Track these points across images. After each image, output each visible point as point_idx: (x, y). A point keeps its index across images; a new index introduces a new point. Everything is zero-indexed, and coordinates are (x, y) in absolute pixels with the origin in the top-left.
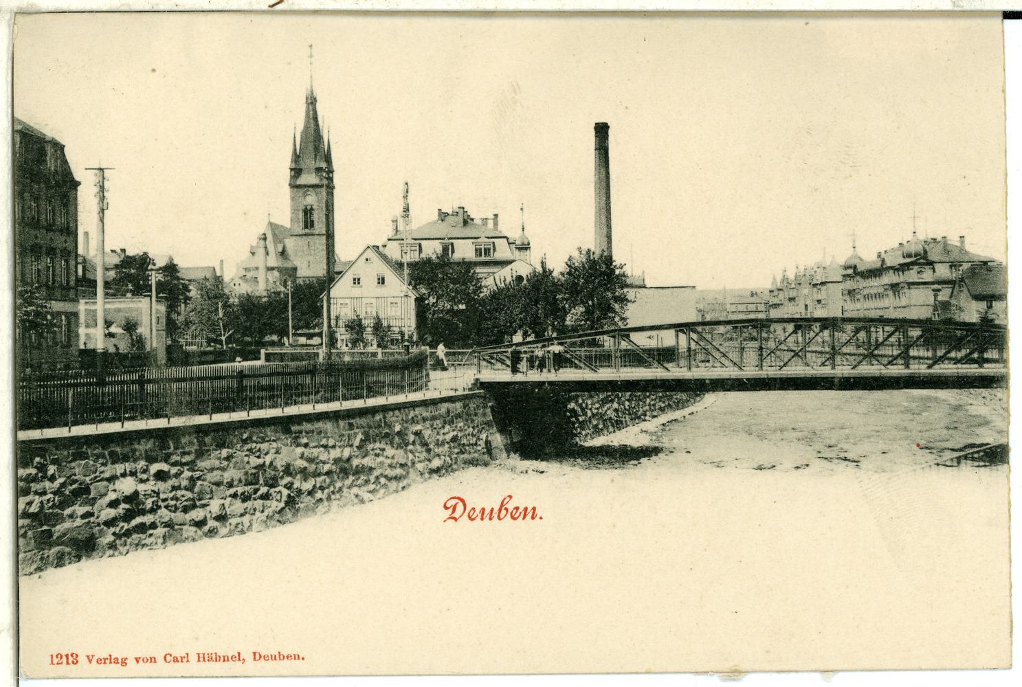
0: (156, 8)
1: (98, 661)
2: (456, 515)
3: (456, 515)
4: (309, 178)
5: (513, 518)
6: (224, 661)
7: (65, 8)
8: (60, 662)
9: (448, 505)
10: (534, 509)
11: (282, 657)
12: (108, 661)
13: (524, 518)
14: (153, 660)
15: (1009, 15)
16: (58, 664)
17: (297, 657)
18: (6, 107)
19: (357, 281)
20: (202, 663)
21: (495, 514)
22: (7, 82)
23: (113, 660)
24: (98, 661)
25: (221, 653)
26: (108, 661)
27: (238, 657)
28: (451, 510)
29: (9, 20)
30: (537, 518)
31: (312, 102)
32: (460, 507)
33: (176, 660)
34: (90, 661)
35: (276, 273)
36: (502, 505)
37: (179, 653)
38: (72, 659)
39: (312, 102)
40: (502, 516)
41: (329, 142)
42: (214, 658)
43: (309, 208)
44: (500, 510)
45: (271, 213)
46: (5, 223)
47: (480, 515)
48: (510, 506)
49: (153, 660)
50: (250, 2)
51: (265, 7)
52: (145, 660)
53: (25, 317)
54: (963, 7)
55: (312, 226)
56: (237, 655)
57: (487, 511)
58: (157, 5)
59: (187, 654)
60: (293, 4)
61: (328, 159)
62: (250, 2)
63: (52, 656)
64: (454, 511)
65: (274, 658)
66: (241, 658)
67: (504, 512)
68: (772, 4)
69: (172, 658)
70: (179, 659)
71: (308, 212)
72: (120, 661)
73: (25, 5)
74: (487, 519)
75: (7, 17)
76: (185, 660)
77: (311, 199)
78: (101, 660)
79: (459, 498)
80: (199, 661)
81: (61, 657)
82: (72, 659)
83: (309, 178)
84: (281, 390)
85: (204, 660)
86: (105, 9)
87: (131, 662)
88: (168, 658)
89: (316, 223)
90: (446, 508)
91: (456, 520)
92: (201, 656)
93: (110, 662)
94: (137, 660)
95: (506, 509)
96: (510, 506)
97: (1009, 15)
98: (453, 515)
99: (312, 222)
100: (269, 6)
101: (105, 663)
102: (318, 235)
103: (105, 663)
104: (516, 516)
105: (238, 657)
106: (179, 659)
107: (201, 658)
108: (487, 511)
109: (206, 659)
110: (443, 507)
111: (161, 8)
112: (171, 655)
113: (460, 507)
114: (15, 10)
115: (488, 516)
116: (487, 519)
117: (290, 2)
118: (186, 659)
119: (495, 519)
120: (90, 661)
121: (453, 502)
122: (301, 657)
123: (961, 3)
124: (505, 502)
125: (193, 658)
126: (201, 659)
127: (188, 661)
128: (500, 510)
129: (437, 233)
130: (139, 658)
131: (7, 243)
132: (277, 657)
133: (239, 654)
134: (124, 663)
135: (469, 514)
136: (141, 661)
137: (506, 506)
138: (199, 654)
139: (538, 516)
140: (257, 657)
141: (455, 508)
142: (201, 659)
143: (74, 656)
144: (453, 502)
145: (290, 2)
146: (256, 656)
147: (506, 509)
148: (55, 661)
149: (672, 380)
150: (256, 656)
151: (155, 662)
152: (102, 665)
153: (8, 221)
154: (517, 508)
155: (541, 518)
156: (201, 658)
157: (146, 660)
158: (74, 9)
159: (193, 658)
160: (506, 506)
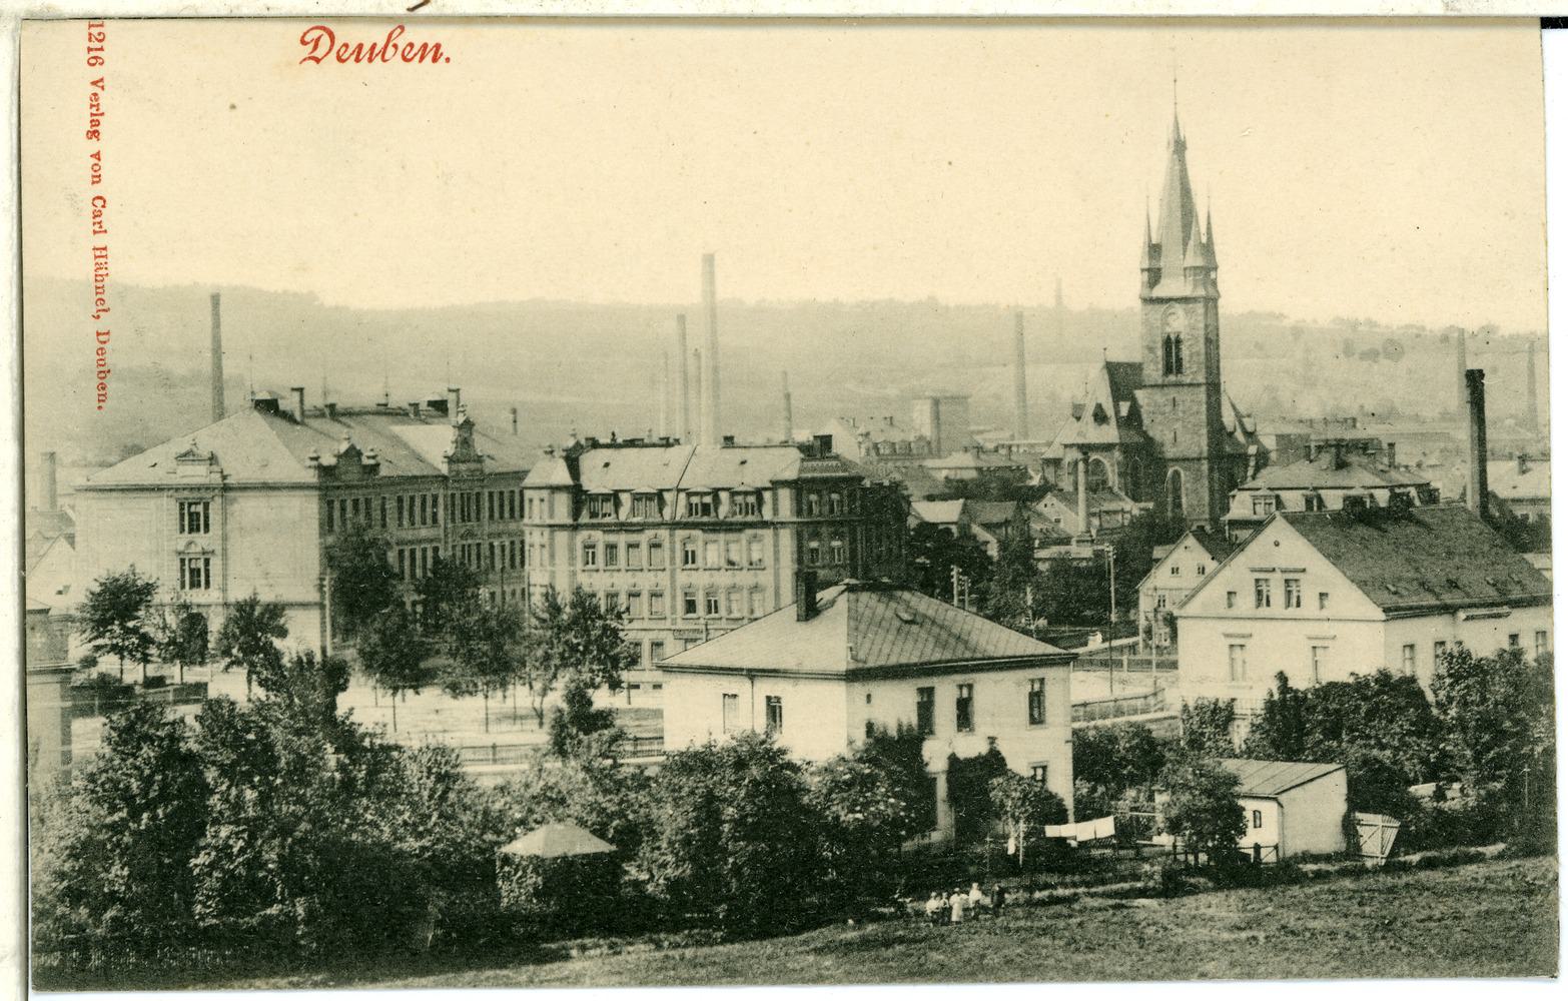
2: (319, 53)
3: (319, 53)
6: (97, 288)
9: (308, 38)
12: (94, 110)
14: (96, 179)
16: (90, 34)
19: (1175, 571)
20: (91, 254)
23: (95, 118)
30: (442, 59)
33: (97, 215)
41: (1209, 223)
42: (100, 272)
43: (1173, 337)
48: (402, 42)
49: (96, 179)
50: (379, 4)
52: (96, 168)
55: (1179, 370)
57: (366, 49)
58: (238, 7)
62: (379, 4)
64: (316, 48)
66: (100, 313)
67: (390, 50)
69: (99, 208)
70: (98, 220)
74: (365, 61)
77: (1179, 322)
78: (103, 389)
85: (96, 257)
87: (94, 146)
88: (99, 203)
89: (1186, 364)
90: (304, 42)
91: (318, 60)
92: (104, 253)
93: (92, 115)
95: (395, 46)
96: (402, 42)
99: (1179, 360)
101: (92, 106)
102: (1190, 385)
103: (92, 106)
104: (409, 57)
106: (98, 220)
108: (366, 49)
109: (98, 260)
112: (104, 206)
113: (326, 39)
115: (432, 53)
116: (365, 61)
117: (440, 3)
118: (98, 230)
120: (94, 83)
121: (316, 34)
122: (101, 404)
124: (394, 36)
125: (101, 241)
126: (98, 253)
127: (95, 232)
130: (99, 159)
132: (102, 369)
138: (105, 249)
140: (102, 338)
142: (98, 253)
143: (101, 37)
144: (316, 34)
145: (440, 3)
147: (395, 46)
151: (93, 183)
157: (96, 168)
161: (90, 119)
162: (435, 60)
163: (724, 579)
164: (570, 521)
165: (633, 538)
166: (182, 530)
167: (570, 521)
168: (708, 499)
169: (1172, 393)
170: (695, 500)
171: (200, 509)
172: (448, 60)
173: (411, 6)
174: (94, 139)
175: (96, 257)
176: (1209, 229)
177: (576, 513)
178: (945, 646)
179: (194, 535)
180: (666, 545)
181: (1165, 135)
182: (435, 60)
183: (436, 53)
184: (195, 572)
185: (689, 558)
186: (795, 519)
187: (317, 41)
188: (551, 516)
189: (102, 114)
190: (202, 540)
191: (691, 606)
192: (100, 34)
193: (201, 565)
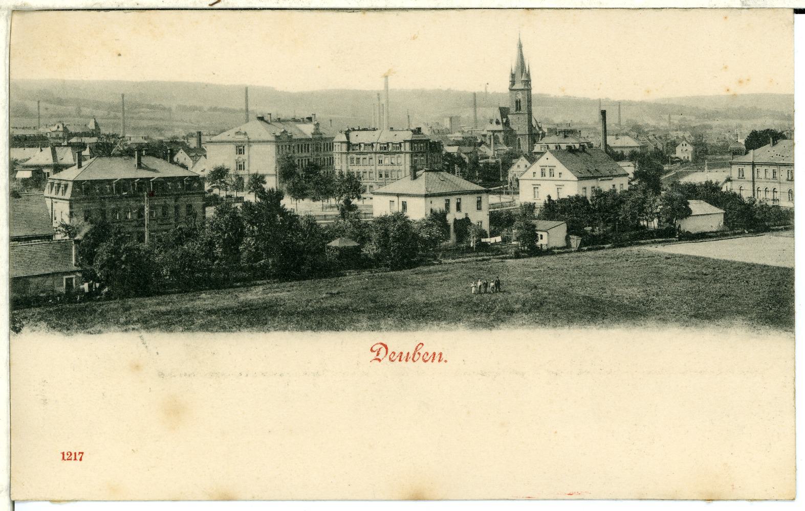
0: (121, 7)
3: (379, 357)
4: (518, 86)
8: (70, 458)
9: (374, 349)
10: (441, 354)
13: (432, 361)
15: (797, 11)
16: (68, 459)
19: (518, 166)
28: (376, 353)
29: (7, 16)
30: (443, 362)
31: (520, 47)
35: (502, 133)
39: (520, 47)
40: (415, 359)
44: (414, 355)
45: (410, 115)
48: (422, 351)
51: (207, 6)
58: (122, 4)
61: (528, 75)
62: (195, 2)
63: (63, 454)
67: (417, 356)
68: (601, 3)
71: (518, 103)
73: (20, 4)
75: (6, 13)
77: (520, 96)
79: (382, 344)
81: (71, 454)
83: (518, 86)
84: (502, 189)
86: (81, 7)
89: (522, 108)
91: (379, 360)
95: (419, 354)
96: (422, 351)
97: (797, 11)
98: (378, 357)
100: (210, 5)
108: (405, 355)
110: (370, 350)
111: (126, 6)
113: (383, 350)
114: (12, 8)
117: (226, 1)
119: (410, 360)
123: (748, 3)
124: (418, 348)
128: (414, 355)
129: (597, 109)
137: (418, 351)
139: (444, 360)
141: (379, 352)
145: (226, 1)
147: (419, 354)
148: (66, 457)
149: (793, 152)
155: (446, 361)
158: (57, 7)
163: (390, 168)
164: (346, 151)
165: (365, 156)
166: (237, 154)
167: (346, 151)
168: (386, 146)
169: (518, 116)
170: (382, 146)
171: (242, 148)
173: (211, 3)
177: (348, 149)
179: (240, 155)
180: (374, 158)
181: (517, 42)
183: (440, 357)
184: (240, 166)
185: (380, 162)
186: (410, 151)
188: (341, 150)
190: (243, 157)
191: (381, 176)
192: (68, 454)
193: (242, 163)
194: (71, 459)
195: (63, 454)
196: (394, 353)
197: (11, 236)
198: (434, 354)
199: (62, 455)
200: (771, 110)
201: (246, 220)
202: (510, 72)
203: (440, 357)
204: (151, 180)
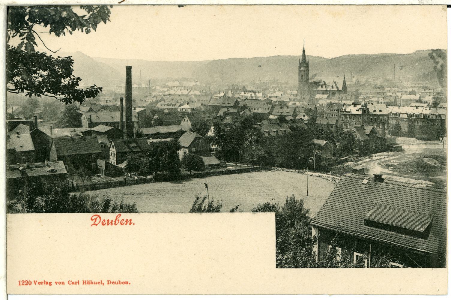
1: (39, 283)
2: (96, 223)
3: (96, 223)
5: (121, 224)
7: (262, 4)
9: (93, 218)
10: (131, 220)
11: (119, 283)
16: (22, 285)
17: (127, 283)
18: (2, 47)
20: (85, 285)
21: (113, 223)
22: (3, 36)
24: (39, 283)
25: (93, 281)
26: (43, 283)
27: (101, 283)
28: (94, 221)
30: (132, 224)
32: (98, 219)
33: (73, 283)
34: (35, 284)
36: (116, 219)
37: (74, 280)
38: (28, 283)
40: (116, 223)
44: (115, 221)
46: (2, 98)
47: (125, 223)
50: (110, 1)
51: (117, 3)
53: (300, 141)
54: (424, 3)
56: (100, 282)
58: (69, 2)
59: (79, 281)
60: (129, 2)
62: (110, 1)
64: (95, 221)
65: (117, 283)
66: (102, 283)
67: (117, 221)
70: (75, 283)
72: (49, 283)
73: (11, 2)
76: (77, 283)
80: (83, 284)
82: (28, 283)
87: (53, 284)
88: (70, 283)
90: (92, 219)
91: (96, 225)
92: (85, 282)
94: (56, 283)
95: (119, 220)
103: (76, 284)
105: (101, 283)
106: (75, 283)
107: (84, 283)
113: (98, 219)
115: (129, 222)
117: (128, 1)
120: (35, 284)
123: (423, 2)
125: (81, 283)
126: (85, 283)
131: (3, 107)
133: (101, 281)
134: (50, 284)
135: (102, 222)
136: (37, 283)
138: (83, 281)
142: (85, 283)
145: (128, 1)
146: (109, 282)
148: (21, 283)
150: (109, 282)
152: (41, 285)
153: (3, 97)
154: (123, 220)
155: (134, 224)
156: (84, 283)
159: (81, 283)
160: (118, 219)
161: (332, 191)
162: (130, 224)
172: (134, 224)
173: (119, 2)
174: (52, 283)
175: (86, 284)
176: (308, 61)
178: (356, 124)
181: (302, 49)
182: (130, 224)
183: (130, 222)
187: (96, 219)
189: (44, 281)
192: (22, 282)
194: (24, 285)
195: (20, 282)
196: (104, 220)
197: (8, 148)
198: (127, 220)
199: (19, 282)
200: (418, 152)
201: (246, 147)
202: (298, 63)
203: (130, 222)
204: (315, 152)
